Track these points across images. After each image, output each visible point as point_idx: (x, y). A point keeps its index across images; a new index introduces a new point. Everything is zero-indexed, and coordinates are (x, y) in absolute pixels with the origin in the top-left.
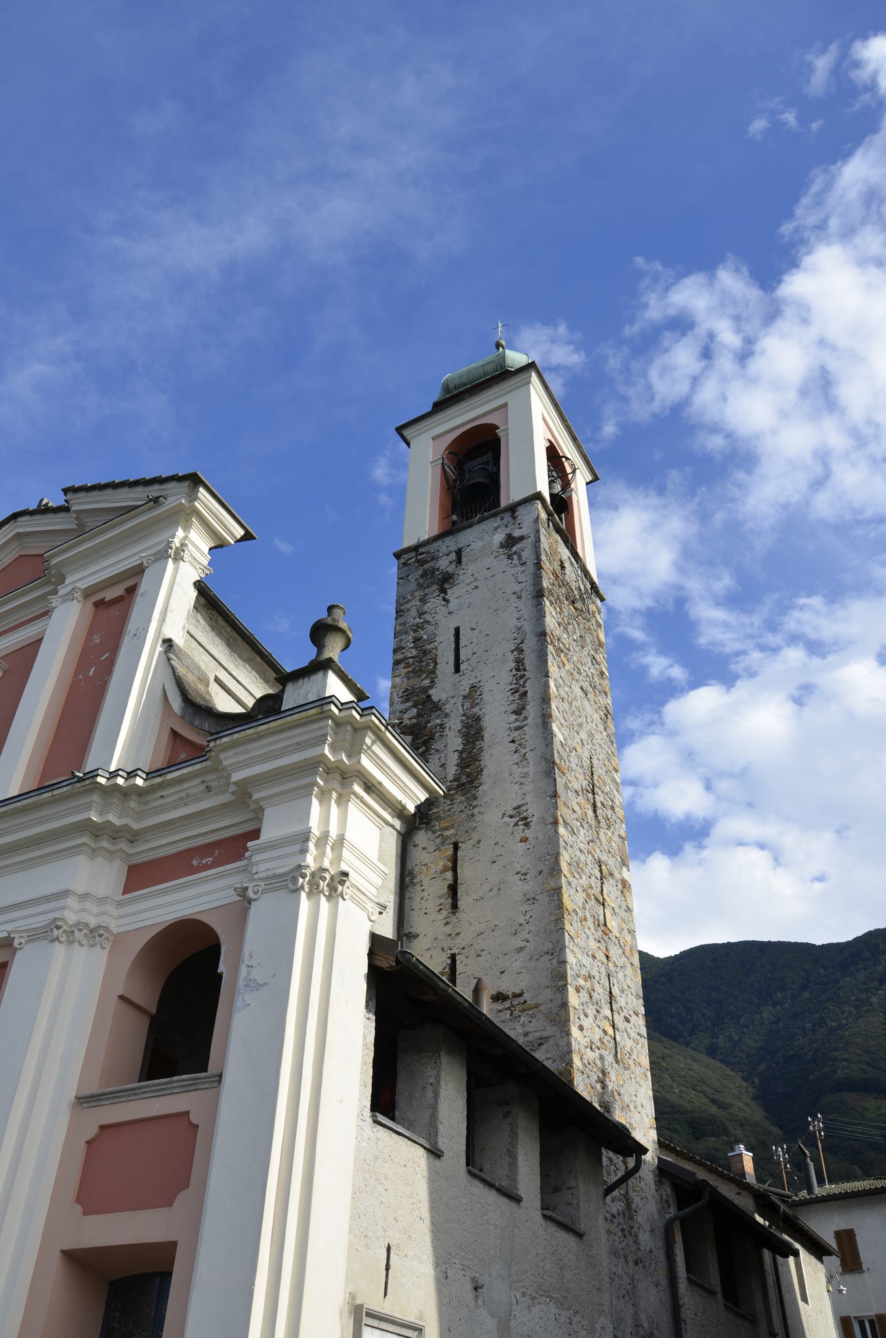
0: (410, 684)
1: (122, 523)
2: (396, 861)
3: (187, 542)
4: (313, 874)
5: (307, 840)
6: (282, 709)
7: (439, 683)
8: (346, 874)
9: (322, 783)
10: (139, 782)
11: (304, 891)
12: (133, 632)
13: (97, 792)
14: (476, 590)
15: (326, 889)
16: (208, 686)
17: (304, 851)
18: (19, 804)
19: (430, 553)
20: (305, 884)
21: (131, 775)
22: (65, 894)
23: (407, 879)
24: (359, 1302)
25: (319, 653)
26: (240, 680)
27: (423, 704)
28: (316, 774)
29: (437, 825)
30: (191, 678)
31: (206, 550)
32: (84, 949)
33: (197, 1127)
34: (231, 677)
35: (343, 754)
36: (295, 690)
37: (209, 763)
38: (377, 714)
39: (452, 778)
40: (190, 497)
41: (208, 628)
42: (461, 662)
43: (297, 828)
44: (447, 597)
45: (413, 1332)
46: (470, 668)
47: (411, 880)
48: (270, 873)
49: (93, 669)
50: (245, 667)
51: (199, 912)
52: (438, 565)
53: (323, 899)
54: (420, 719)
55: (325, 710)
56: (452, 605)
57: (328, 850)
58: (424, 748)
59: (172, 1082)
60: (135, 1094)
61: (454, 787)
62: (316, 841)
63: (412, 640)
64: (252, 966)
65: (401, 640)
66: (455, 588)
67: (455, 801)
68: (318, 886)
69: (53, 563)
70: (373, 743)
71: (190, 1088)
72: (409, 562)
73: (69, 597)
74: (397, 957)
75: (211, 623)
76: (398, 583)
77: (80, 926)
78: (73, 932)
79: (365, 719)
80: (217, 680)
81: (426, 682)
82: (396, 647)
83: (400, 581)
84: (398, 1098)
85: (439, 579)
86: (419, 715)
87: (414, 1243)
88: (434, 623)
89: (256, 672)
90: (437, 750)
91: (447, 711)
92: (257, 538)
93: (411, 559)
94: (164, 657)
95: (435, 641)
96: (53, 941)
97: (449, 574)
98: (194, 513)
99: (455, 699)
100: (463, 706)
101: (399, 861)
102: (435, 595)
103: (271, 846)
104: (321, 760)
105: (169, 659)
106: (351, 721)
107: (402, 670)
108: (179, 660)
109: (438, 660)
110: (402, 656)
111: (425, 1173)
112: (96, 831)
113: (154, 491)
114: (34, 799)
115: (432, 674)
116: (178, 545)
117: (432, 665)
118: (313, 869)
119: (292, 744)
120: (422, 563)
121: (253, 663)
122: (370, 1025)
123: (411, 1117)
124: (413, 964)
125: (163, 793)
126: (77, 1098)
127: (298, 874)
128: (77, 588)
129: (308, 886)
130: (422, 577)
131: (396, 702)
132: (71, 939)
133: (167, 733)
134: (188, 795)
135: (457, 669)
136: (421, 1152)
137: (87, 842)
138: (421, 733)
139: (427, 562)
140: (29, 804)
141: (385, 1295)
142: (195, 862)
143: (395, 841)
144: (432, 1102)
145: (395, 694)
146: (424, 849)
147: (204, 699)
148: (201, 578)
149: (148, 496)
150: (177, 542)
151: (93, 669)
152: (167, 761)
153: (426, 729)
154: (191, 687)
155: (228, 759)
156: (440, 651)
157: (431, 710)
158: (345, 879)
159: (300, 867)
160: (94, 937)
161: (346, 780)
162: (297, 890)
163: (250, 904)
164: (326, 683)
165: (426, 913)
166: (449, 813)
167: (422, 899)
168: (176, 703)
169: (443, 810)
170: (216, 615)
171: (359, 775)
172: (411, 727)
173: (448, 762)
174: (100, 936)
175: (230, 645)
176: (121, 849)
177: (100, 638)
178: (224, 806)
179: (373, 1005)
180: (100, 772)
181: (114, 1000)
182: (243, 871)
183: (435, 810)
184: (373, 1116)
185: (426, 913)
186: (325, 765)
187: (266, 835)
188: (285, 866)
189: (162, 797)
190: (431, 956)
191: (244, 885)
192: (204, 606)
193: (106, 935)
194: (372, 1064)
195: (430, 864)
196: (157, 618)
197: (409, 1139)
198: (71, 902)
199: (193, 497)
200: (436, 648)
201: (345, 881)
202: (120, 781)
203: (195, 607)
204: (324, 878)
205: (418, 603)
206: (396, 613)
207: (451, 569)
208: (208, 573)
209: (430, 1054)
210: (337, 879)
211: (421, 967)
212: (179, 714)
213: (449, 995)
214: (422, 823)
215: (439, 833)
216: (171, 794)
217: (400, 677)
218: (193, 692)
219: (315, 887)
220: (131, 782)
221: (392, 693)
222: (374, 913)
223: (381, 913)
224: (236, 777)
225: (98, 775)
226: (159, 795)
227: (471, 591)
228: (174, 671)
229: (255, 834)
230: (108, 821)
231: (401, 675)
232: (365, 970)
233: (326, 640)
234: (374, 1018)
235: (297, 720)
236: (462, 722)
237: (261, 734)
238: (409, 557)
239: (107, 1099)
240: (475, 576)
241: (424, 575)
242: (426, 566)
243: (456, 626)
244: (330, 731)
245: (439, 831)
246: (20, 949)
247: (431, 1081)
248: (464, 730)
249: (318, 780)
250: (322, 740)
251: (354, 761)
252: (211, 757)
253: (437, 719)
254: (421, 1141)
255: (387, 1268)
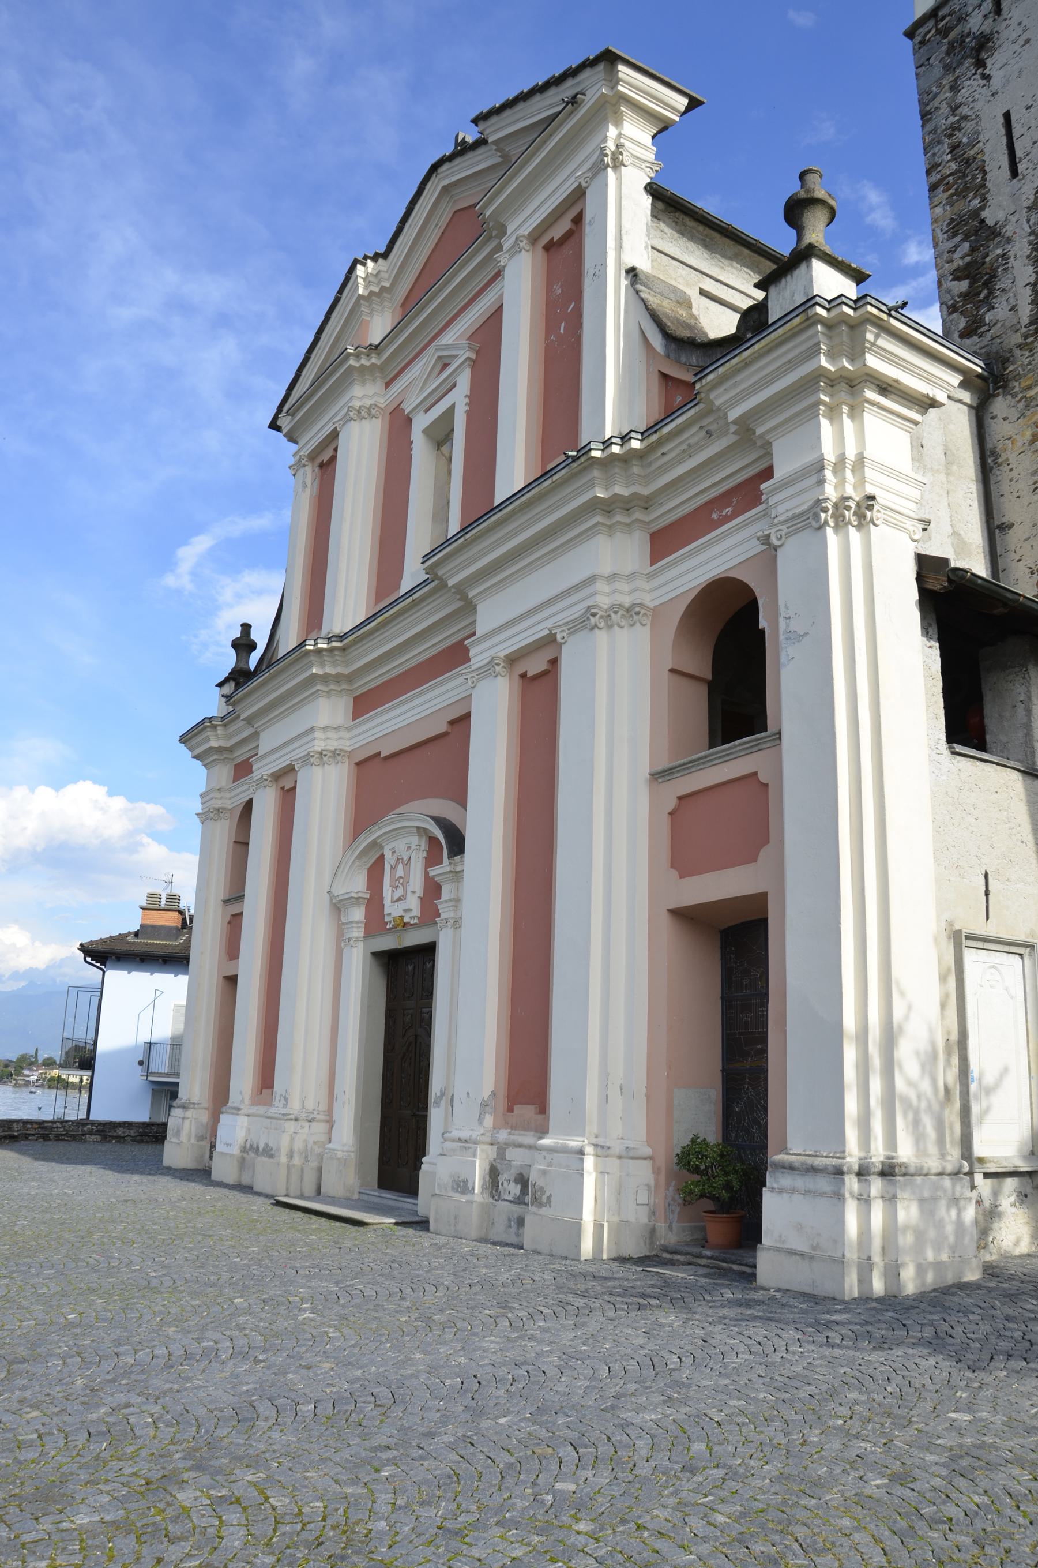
0: (954, 212)
1: (545, 142)
2: (972, 442)
3: (622, 141)
4: (836, 506)
5: (822, 468)
6: (770, 323)
7: (992, 200)
8: (872, 498)
9: (827, 399)
10: (635, 444)
11: (829, 526)
12: (591, 272)
13: (595, 466)
14: (1027, 45)
15: (853, 519)
16: (690, 308)
17: (821, 482)
18: (523, 499)
19: (955, 12)
20: (829, 518)
21: (625, 439)
22: (592, 579)
23: (990, 460)
24: (957, 927)
25: (800, 237)
26: (731, 283)
27: (976, 233)
28: (817, 390)
29: (1016, 386)
30: (668, 306)
31: (647, 140)
32: (625, 631)
33: (767, 785)
34: (719, 284)
35: (844, 360)
36: (779, 294)
37: (701, 406)
38: (873, 302)
39: (1027, 322)
40: (611, 81)
41: (676, 235)
42: (1017, 160)
43: (809, 458)
44: (987, 72)
45: (1024, 949)
46: (1031, 165)
47: (994, 460)
48: (790, 514)
49: (563, 325)
50: (732, 267)
51: (729, 569)
52: (968, 26)
53: (852, 530)
54: (976, 254)
55: (810, 315)
56: (996, 82)
57: (849, 474)
58: (985, 292)
59: (735, 746)
60: (703, 763)
61: (1031, 332)
62: (833, 468)
63: (948, 151)
64: (790, 618)
65: (934, 154)
66: (996, 53)
67: (1035, 351)
68: (844, 517)
69: (487, 214)
70: (877, 336)
71: (754, 750)
72: (927, 38)
73: (515, 250)
74: (949, 577)
75: (678, 228)
76: (917, 74)
77: (615, 608)
78: (609, 616)
79: (860, 312)
80: (703, 293)
81: (976, 203)
82: (928, 166)
83: (919, 70)
84: (987, 721)
85: (972, 49)
86: (973, 250)
87: (1017, 867)
88: (973, 117)
89: (748, 267)
90: (1003, 290)
91: (1009, 234)
92: (705, 101)
93: (929, 31)
94: (631, 290)
95: (979, 142)
96: (592, 629)
97: (985, 36)
98: (621, 101)
99: (1017, 216)
100: (1028, 221)
101: (976, 441)
102: (969, 74)
103: (786, 484)
104: (821, 373)
105: (637, 292)
106: (844, 319)
107: (942, 195)
108: (649, 288)
109: (986, 168)
110: (939, 176)
111: (1023, 796)
112: (607, 507)
113: (567, 89)
114: (537, 490)
115: (981, 189)
116: (613, 148)
117: (980, 176)
118: (834, 500)
119: (784, 364)
120: (945, 32)
121: (740, 258)
122: (934, 653)
123: (1003, 738)
124: (969, 580)
125: (664, 450)
126: (651, 775)
127: (818, 509)
128: (521, 236)
129: (833, 520)
130: (948, 53)
131: (941, 239)
132: (609, 623)
133: (656, 378)
134: (689, 446)
135: (1014, 173)
136: (1015, 776)
137: (601, 521)
138: (980, 273)
139: (952, 29)
140: (532, 497)
141: (987, 918)
142: (715, 516)
143: (967, 418)
144: (1025, 721)
145: (938, 231)
146: (1004, 419)
147: (689, 327)
148: (651, 178)
149: (563, 100)
150: (611, 146)
151: (563, 325)
152: (663, 410)
153: (985, 266)
154: (668, 317)
155: (719, 398)
156: (987, 155)
157: (988, 239)
158: (872, 503)
159: (819, 501)
160: (632, 616)
161: (855, 388)
162: (821, 527)
163: (776, 550)
164: (812, 276)
165: (1018, 497)
166: (1029, 367)
167: (1011, 480)
168: (657, 342)
169: (1022, 365)
170: (681, 216)
171: (869, 379)
172: (965, 268)
173: (1018, 302)
174: (638, 613)
175: (707, 245)
176: (637, 520)
177: (561, 287)
178: (730, 448)
179: (934, 631)
180: (592, 446)
181: (666, 674)
182: (764, 515)
183: (1011, 368)
184: (950, 748)
185: (1018, 497)
186: (826, 377)
187: (780, 472)
188: (802, 504)
189: (663, 454)
190: (1032, 546)
191: (766, 533)
192: (663, 211)
193: (643, 611)
194: (941, 695)
195: (1015, 437)
196: (613, 246)
197: (998, 764)
198: (601, 586)
199: (614, 81)
200: (982, 151)
201: (873, 505)
202: (616, 449)
203: (654, 216)
204: (848, 508)
205: (948, 95)
206: (922, 118)
207: (986, 28)
208: (658, 169)
209: (1017, 669)
210: (864, 505)
211: (980, 581)
212: (662, 353)
213: (1022, 604)
214: (998, 388)
215: (1020, 396)
216: (671, 450)
217: (941, 205)
218: (672, 323)
219: (841, 519)
220: (627, 447)
221: (933, 230)
222: (916, 531)
223: (924, 530)
224: (733, 414)
225: (590, 450)
226: (660, 453)
227: (1020, 50)
228: (645, 305)
229: (768, 473)
230: (616, 494)
231: (941, 203)
232: (916, 596)
233: (804, 220)
234: (937, 645)
235: (782, 335)
236: (1030, 243)
237: (747, 360)
238: (927, 29)
239: (678, 771)
240: (1023, 25)
241: (951, 47)
242: (952, 35)
243: (1004, 111)
244: (821, 337)
245: (1021, 392)
246: (564, 643)
247: (1021, 698)
248: (1035, 253)
249: (822, 397)
250: (815, 351)
251: (858, 364)
252: (701, 399)
253: (998, 248)
254: (1012, 764)
255: (987, 894)
